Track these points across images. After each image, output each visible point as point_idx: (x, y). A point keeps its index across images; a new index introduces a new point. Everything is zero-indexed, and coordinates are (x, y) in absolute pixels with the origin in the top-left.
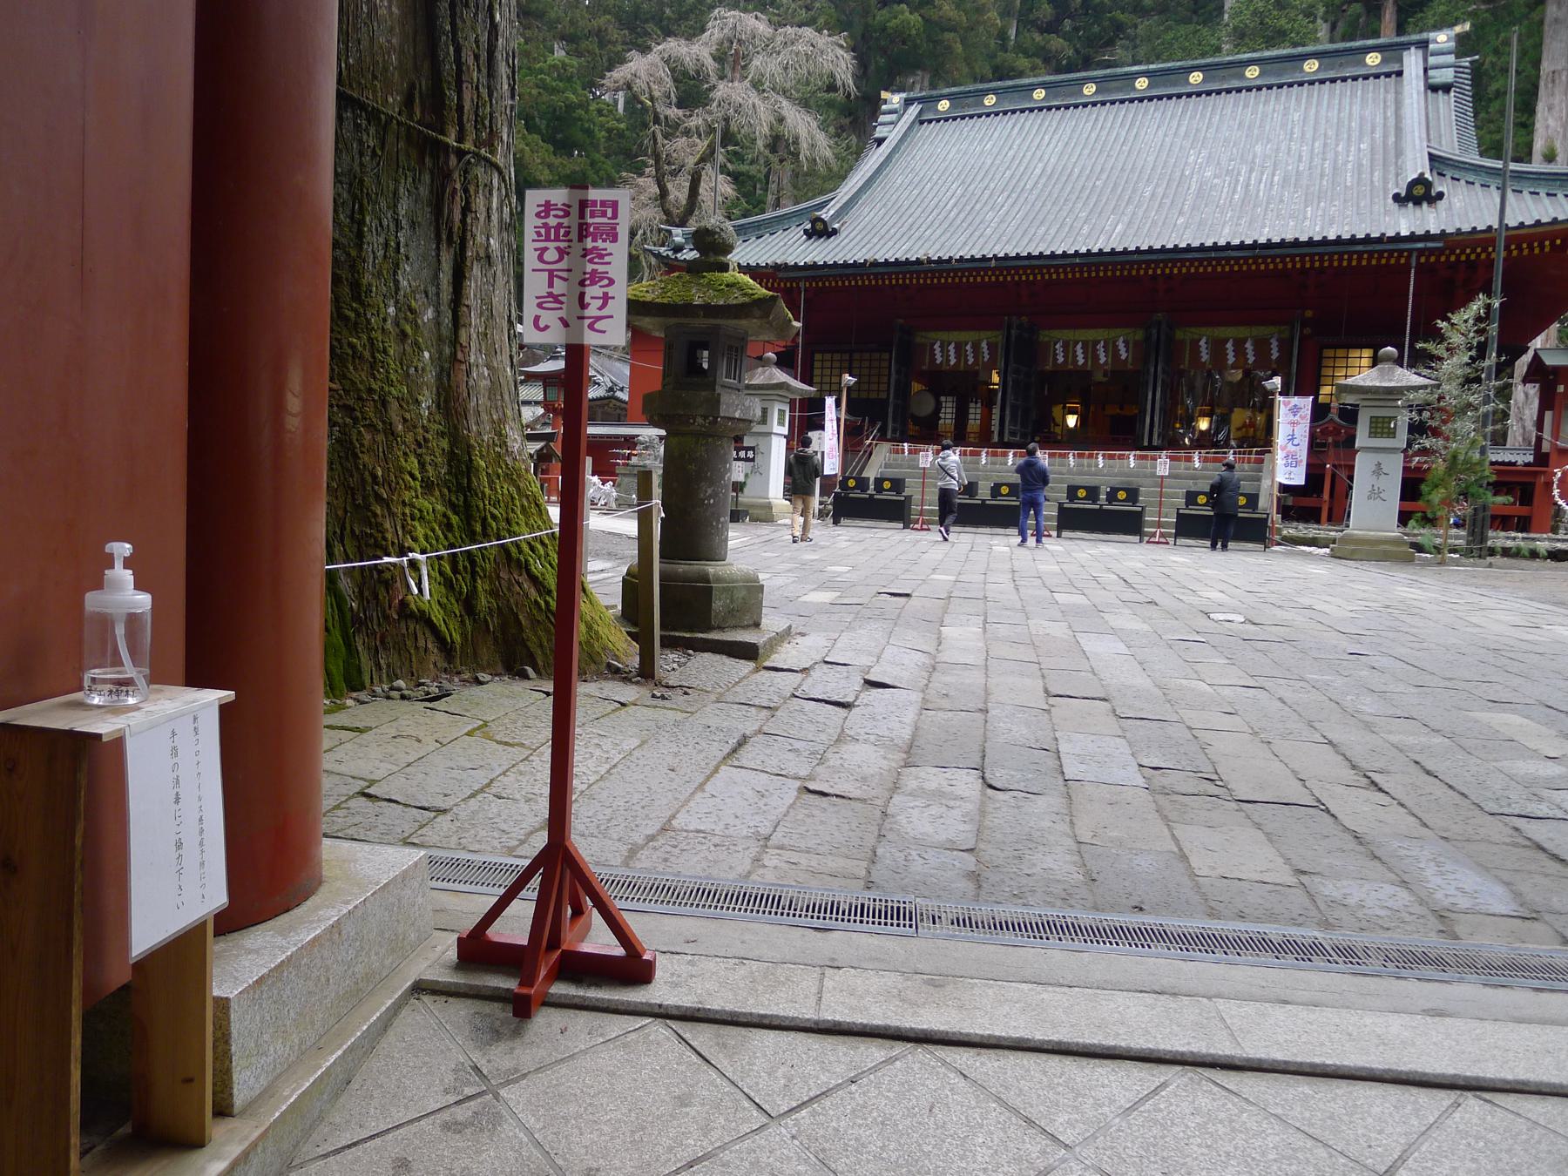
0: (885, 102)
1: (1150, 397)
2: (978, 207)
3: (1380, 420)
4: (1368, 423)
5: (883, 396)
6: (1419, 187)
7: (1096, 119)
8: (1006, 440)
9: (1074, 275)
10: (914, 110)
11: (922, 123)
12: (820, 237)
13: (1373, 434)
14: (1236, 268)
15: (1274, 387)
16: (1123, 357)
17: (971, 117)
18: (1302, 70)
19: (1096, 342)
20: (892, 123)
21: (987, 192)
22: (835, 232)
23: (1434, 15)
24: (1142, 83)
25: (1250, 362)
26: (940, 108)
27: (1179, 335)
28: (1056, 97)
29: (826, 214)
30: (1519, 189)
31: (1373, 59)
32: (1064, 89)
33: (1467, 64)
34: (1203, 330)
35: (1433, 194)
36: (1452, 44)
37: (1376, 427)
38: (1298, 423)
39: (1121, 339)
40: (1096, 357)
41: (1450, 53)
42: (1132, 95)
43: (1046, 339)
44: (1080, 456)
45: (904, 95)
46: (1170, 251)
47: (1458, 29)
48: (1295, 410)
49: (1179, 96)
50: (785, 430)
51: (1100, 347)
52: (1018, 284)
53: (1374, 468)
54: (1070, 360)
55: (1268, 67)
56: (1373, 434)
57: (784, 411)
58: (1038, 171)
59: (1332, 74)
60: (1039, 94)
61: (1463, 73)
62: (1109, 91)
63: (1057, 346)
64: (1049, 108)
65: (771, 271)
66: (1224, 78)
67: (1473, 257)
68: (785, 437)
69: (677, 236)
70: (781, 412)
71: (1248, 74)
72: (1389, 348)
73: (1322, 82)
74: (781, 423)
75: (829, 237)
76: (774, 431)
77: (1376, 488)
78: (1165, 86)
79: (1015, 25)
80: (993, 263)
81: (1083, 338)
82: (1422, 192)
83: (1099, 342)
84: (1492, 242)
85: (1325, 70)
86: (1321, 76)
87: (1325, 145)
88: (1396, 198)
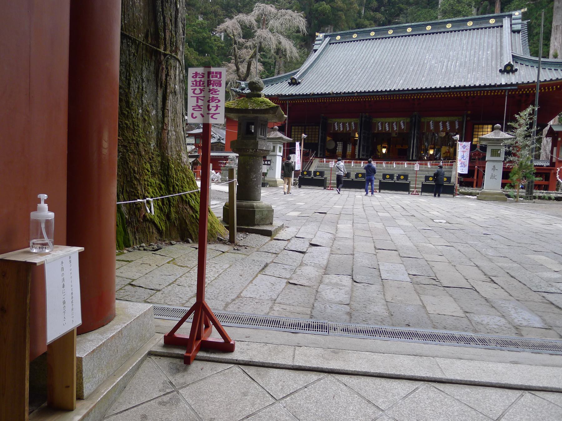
0: (317, 36)
1: (412, 142)
2: (351, 74)
3: (495, 150)
4: (490, 152)
5: (317, 142)
6: (509, 67)
7: (393, 43)
8: (361, 157)
9: (385, 98)
10: (328, 39)
11: (330, 44)
12: (294, 85)
13: (492, 155)
14: (443, 96)
15: (457, 139)
16: (403, 128)
17: (348, 42)
18: (467, 25)
19: (393, 123)
20: (320, 44)
21: (354, 69)
22: (299, 83)
24: (409, 30)
25: (448, 129)
26: (337, 39)
28: (378, 35)
29: (296, 77)
30: (545, 68)
31: (492, 21)
32: (381, 32)
33: (526, 23)
34: (431, 118)
35: (514, 69)
36: (521, 16)
37: (493, 153)
38: (465, 152)
39: (402, 121)
40: (393, 128)
41: (520, 19)
42: (406, 34)
43: (375, 121)
44: (387, 163)
45: (324, 34)
46: (419, 90)
47: (523, 10)
48: (464, 147)
49: (423, 34)
50: (281, 154)
51: (394, 124)
52: (365, 102)
53: (492, 168)
54: (384, 129)
55: (455, 24)
56: (492, 155)
57: (281, 147)
58: (372, 61)
59: (477, 27)
60: (373, 34)
61: (524, 26)
62: (397, 33)
63: (379, 124)
65: (276, 97)
66: (439, 28)
67: (528, 92)
68: (281, 156)
69: (243, 84)
70: (280, 148)
71: (447, 27)
72: (498, 125)
73: (474, 29)
74: (280, 151)
75: (297, 85)
76: (278, 154)
77: (493, 175)
78: (418, 31)
80: (356, 94)
81: (388, 121)
82: (510, 69)
83: (394, 122)
84: (535, 86)
85: (475, 25)
86: (474, 27)
88: (501, 71)
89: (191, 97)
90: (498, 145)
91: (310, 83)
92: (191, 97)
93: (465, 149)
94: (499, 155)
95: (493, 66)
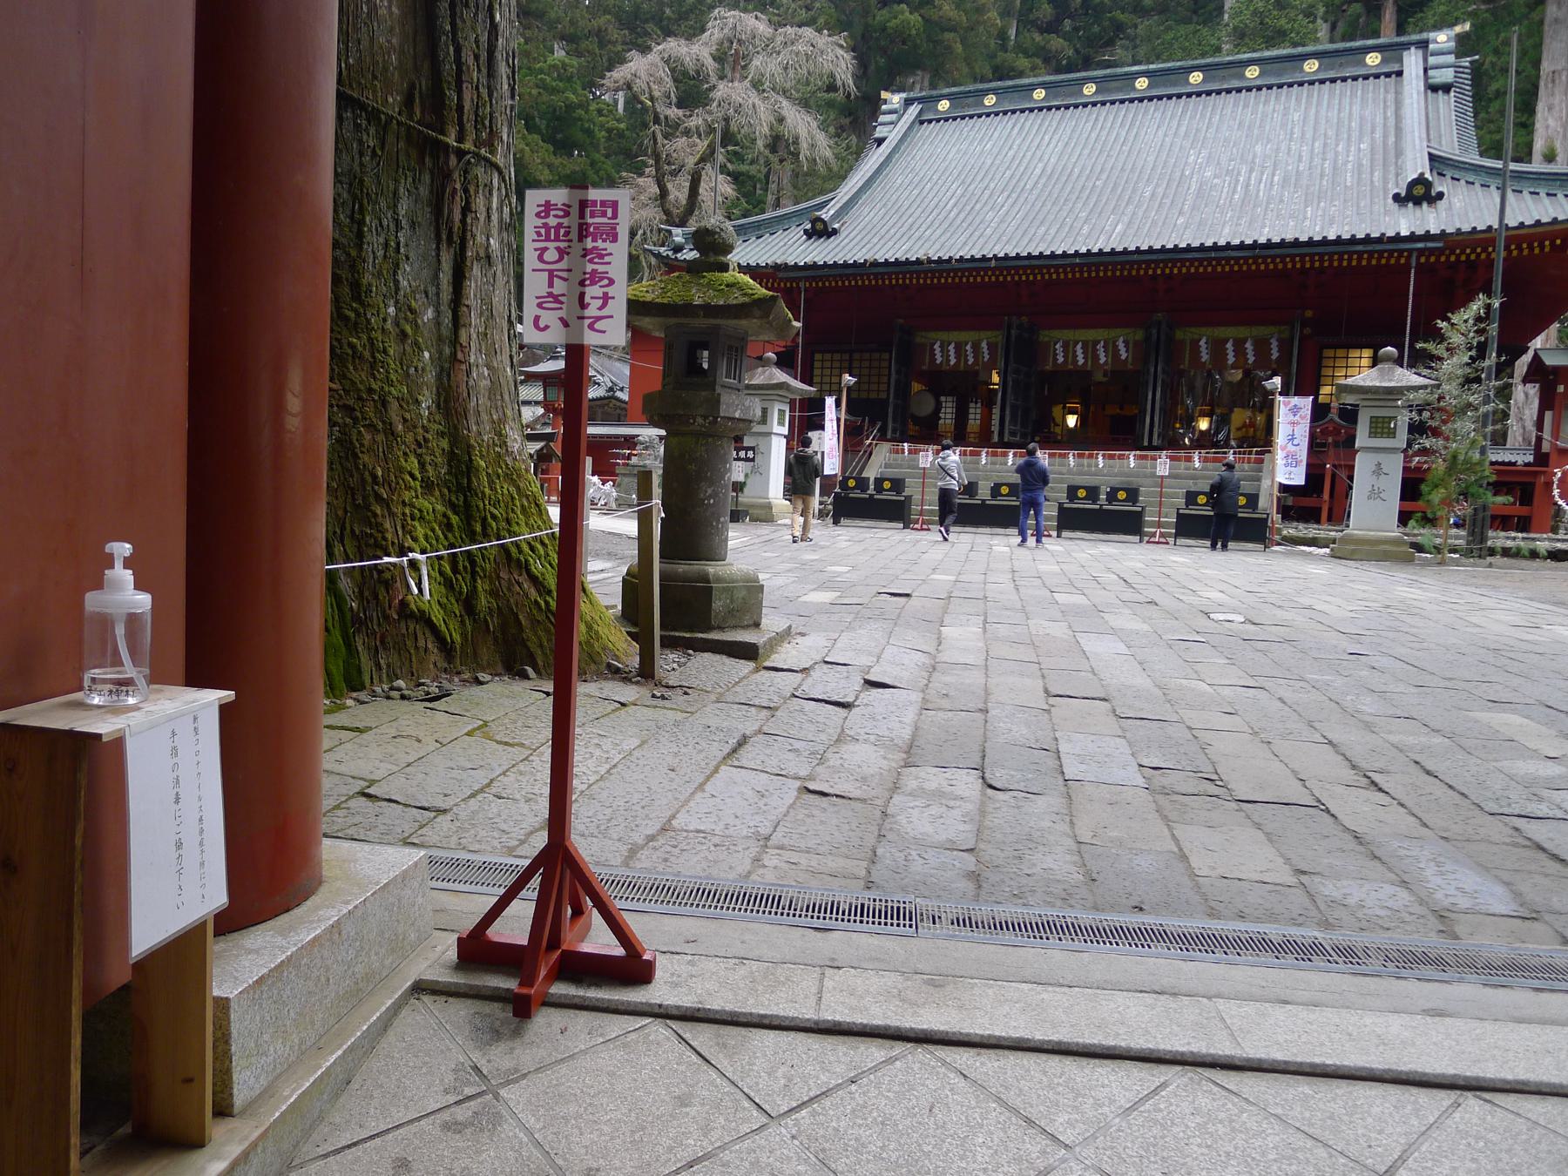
0: (885, 102)
1: (1150, 397)
2: (978, 207)
3: (1380, 420)
4: (1368, 423)
6: (1419, 187)
7: (1096, 119)
8: (1006, 440)
9: (1074, 275)
10: (914, 110)
11: (922, 123)
12: (820, 237)
13: (1373, 434)
14: (1236, 268)
15: (1274, 387)
16: (1123, 357)
17: (971, 117)
18: (1302, 70)
19: (1096, 342)
20: (892, 123)
21: (987, 192)
22: (835, 232)
23: (1434, 15)
24: (1142, 83)
25: (1250, 362)
26: (940, 108)
27: (1179, 335)
28: (1056, 97)
29: (826, 214)
30: (1519, 189)
31: (1373, 59)
32: (1064, 89)
33: (1467, 64)
34: (1203, 330)
35: (1433, 194)
36: (1452, 44)
37: (1376, 427)
38: (1298, 423)
39: (1121, 339)
40: (1096, 357)
41: (1450, 53)
42: (1132, 95)
43: (1046, 339)
44: (1080, 456)
45: (904, 95)
47: (1458, 29)
48: (1295, 410)
49: (1179, 96)
50: (785, 430)
51: (1100, 347)
52: (1018, 284)
53: (1374, 468)
54: (1070, 360)
55: (1268, 67)
56: (1373, 434)
57: (784, 411)
58: (1038, 171)
59: (1332, 74)
60: (1039, 94)
61: (1463, 73)
62: (1109, 91)
63: (1057, 346)
64: (1049, 108)
65: (771, 271)
66: (1224, 78)
67: (1473, 257)
68: (785, 437)
69: (677, 236)
70: (781, 412)
71: (1248, 74)
72: (1389, 348)
73: (1322, 82)
74: (781, 423)
75: (829, 237)
76: (774, 431)
77: (1376, 488)
78: (1165, 86)
79: (1015, 25)
80: (993, 263)
81: (1083, 338)
82: (1422, 192)
83: (1099, 342)
84: (1492, 242)
85: (1325, 70)
86: (1321, 76)
87: (1325, 145)
88: (1396, 198)
89: (533, 270)
90: (1389, 404)
91: (864, 233)
92: (533, 270)
93: (1297, 418)
94: (1392, 434)
95: (1377, 184)
